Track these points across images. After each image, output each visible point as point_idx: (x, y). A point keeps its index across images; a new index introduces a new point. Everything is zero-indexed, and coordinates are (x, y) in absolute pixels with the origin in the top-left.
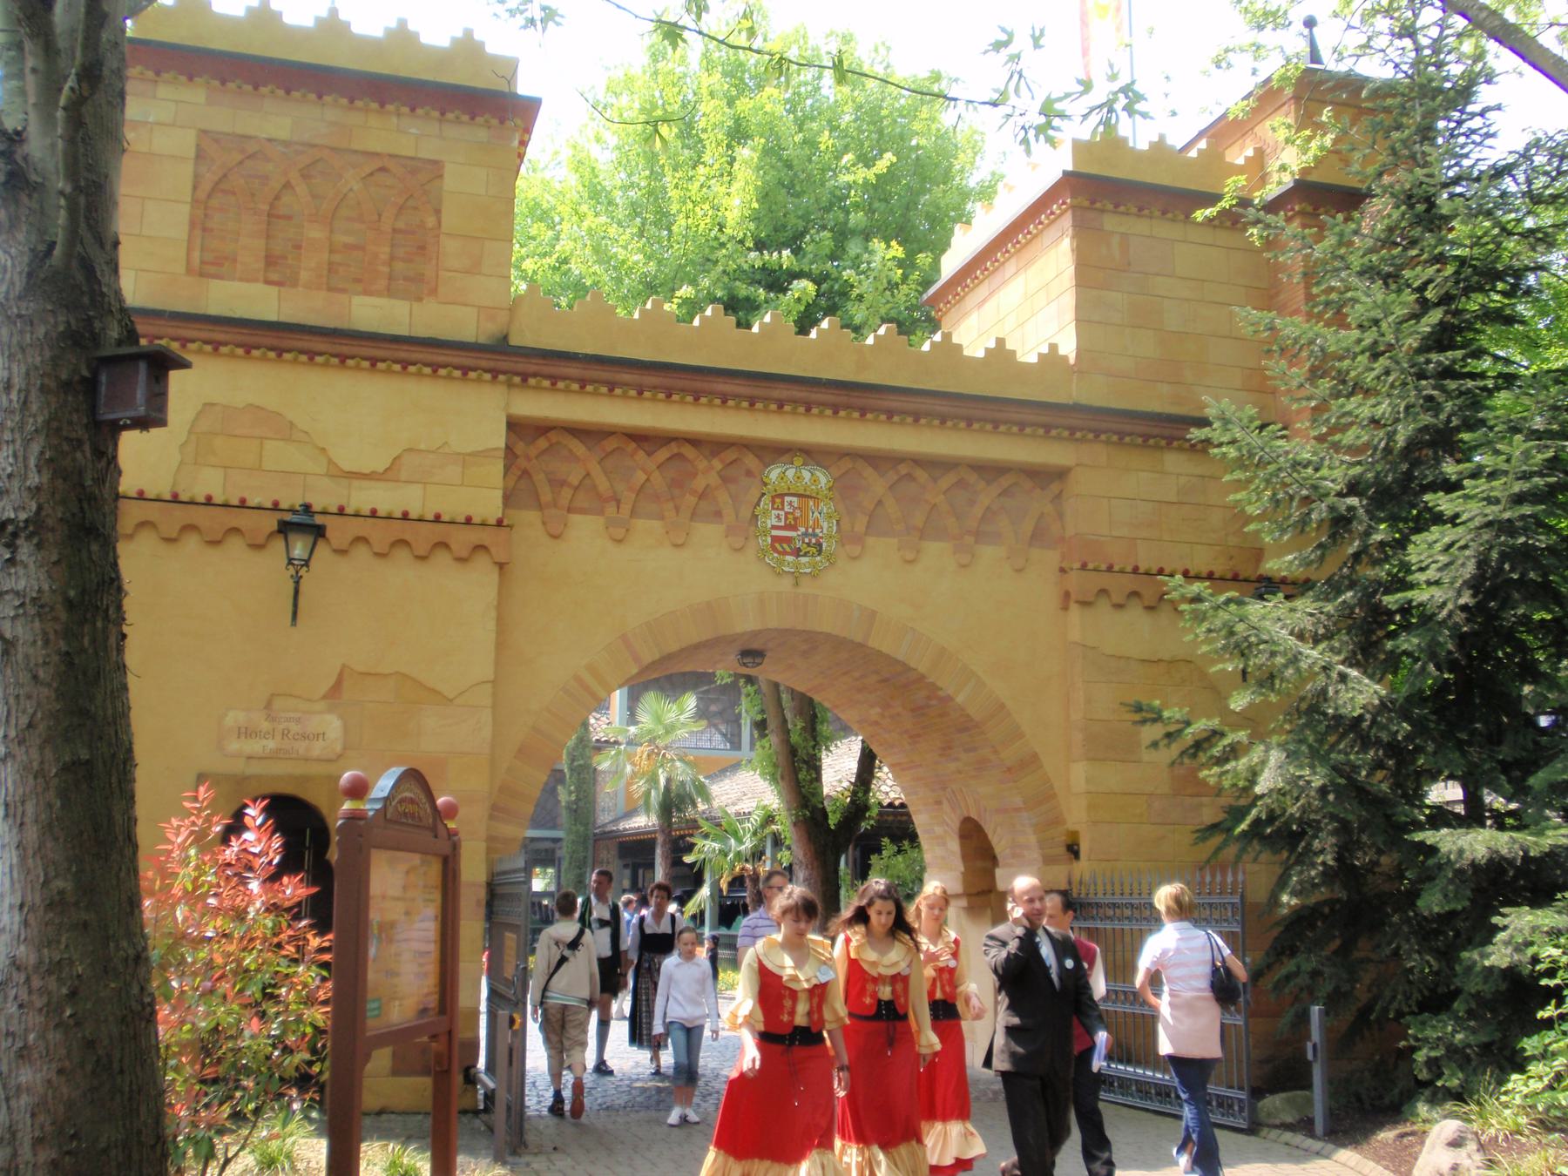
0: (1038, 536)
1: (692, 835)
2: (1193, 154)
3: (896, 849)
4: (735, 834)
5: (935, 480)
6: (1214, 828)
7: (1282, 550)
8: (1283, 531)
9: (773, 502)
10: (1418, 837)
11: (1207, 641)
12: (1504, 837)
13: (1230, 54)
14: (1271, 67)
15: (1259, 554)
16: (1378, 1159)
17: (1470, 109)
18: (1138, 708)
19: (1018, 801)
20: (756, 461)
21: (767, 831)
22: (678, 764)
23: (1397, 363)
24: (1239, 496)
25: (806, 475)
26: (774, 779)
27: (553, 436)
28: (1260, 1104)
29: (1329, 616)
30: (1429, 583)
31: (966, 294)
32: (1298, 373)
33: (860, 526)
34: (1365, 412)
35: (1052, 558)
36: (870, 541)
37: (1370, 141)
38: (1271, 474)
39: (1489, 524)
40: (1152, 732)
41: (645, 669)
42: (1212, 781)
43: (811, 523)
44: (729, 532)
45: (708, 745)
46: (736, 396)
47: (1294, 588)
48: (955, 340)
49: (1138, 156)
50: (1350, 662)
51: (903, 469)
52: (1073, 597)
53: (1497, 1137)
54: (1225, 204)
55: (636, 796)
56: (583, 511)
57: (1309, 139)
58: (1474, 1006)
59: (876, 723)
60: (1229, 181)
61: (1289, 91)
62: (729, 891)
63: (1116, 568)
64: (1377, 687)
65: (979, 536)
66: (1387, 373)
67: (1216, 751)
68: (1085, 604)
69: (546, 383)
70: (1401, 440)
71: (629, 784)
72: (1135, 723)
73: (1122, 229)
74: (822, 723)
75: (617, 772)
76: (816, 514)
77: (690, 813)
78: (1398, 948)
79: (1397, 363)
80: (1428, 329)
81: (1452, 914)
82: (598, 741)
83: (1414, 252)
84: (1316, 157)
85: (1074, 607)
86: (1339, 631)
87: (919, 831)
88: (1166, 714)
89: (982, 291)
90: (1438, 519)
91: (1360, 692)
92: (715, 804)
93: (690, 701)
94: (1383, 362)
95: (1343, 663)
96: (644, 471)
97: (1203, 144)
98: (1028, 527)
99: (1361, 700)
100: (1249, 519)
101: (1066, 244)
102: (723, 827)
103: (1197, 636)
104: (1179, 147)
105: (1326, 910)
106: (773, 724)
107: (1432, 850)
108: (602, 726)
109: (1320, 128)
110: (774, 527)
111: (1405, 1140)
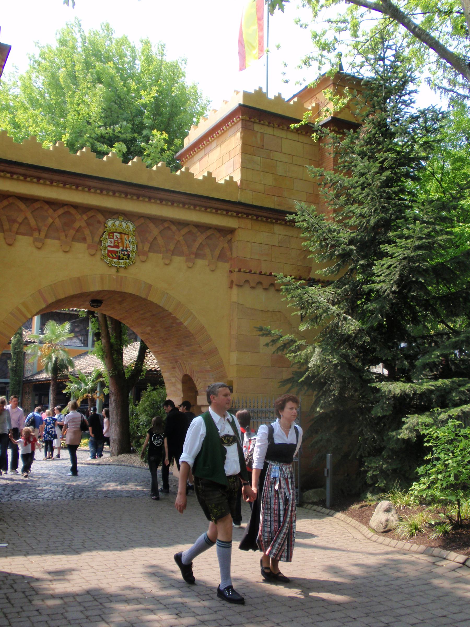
0: (222, 257)
1: (65, 382)
2: (292, 103)
3: (153, 388)
4: (84, 381)
5: (179, 230)
6: (288, 381)
7: (321, 266)
8: (324, 258)
9: (109, 235)
10: (374, 385)
11: (291, 302)
12: (407, 386)
13: (310, 60)
14: (326, 68)
15: (309, 269)
16: (353, 517)
17: (404, 92)
18: (261, 329)
19: (208, 368)
20: (102, 217)
21: (98, 380)
22: (61, 351)
23: (372, 191)
24: (306, 243)
25: (124, 224)
26: (103, 358)
27: (11, 200)
28: (304, 494)
29: (339, 295)
30: (380, 282)
31: (194, 155)
32: (332, 193)
33: (146, 248)
34: (358, 211)
35: (227, 266)
36: (151, 254)
37: (364, 101)
38: (320, 234)
39: (405, 258)
40: (267, 339)
41: (49, 306)
42: (290, 359)
43: (125, 245)
44: (89, 247)
45: (74, 344)
46: (95, 188)
47: (326, 283)
48: (191, 171)
49: (270, 101)
50: (347, 313)
51: (166, 225)
52: (235, 283)
53: (400, 507)
54: (303, 123)
55: (42, 364)
56: (23, 234)
57: (338, 100)
58: (390, 453)
59: (149, 334)
60: (305, 113)
61: (332, 78)
62: (81, 406)
63: (253, 272)
64: (358, 323)
65: (197, 255)
66: (368, 195)
67: (292, 348)
68: (239, 286)
69: (8, 175)
70: (372, 223)
71: (39, 360)
72: (259, 335)
73: (262, 131)
74: (124, 334)
75: (34, 354)
76: (128, 242)
77: (65, 372)
78: (362, 430)
79: (372, 191)
80: (385, 178)
81: (384, 417)
82: (26, 341)
83: (380, 147)
84: (340, 107)
85: (234, 287)
86: (343, 301)
87: (165, 380)
88: (273, 332)
89: (202, 153)
90: (386, 255)
91: (352, 325)
92: (76, 369)
93: (67, 325)
94: (367, 190)
95: (344, 313)
96: (52, 218)
97: (295, 99)
98: (217, 252)
99: (352, 327)
100: (311, 252)
101: (238, 135)
102: (79, 378)
103: (287, 299)
104: (286, 100)
105: (331, 415)
106: (103, 334)
107: (378, 390)
108: (27, 335)
109: (342, 95)
110: (109, 246)
111: (363, 508)
